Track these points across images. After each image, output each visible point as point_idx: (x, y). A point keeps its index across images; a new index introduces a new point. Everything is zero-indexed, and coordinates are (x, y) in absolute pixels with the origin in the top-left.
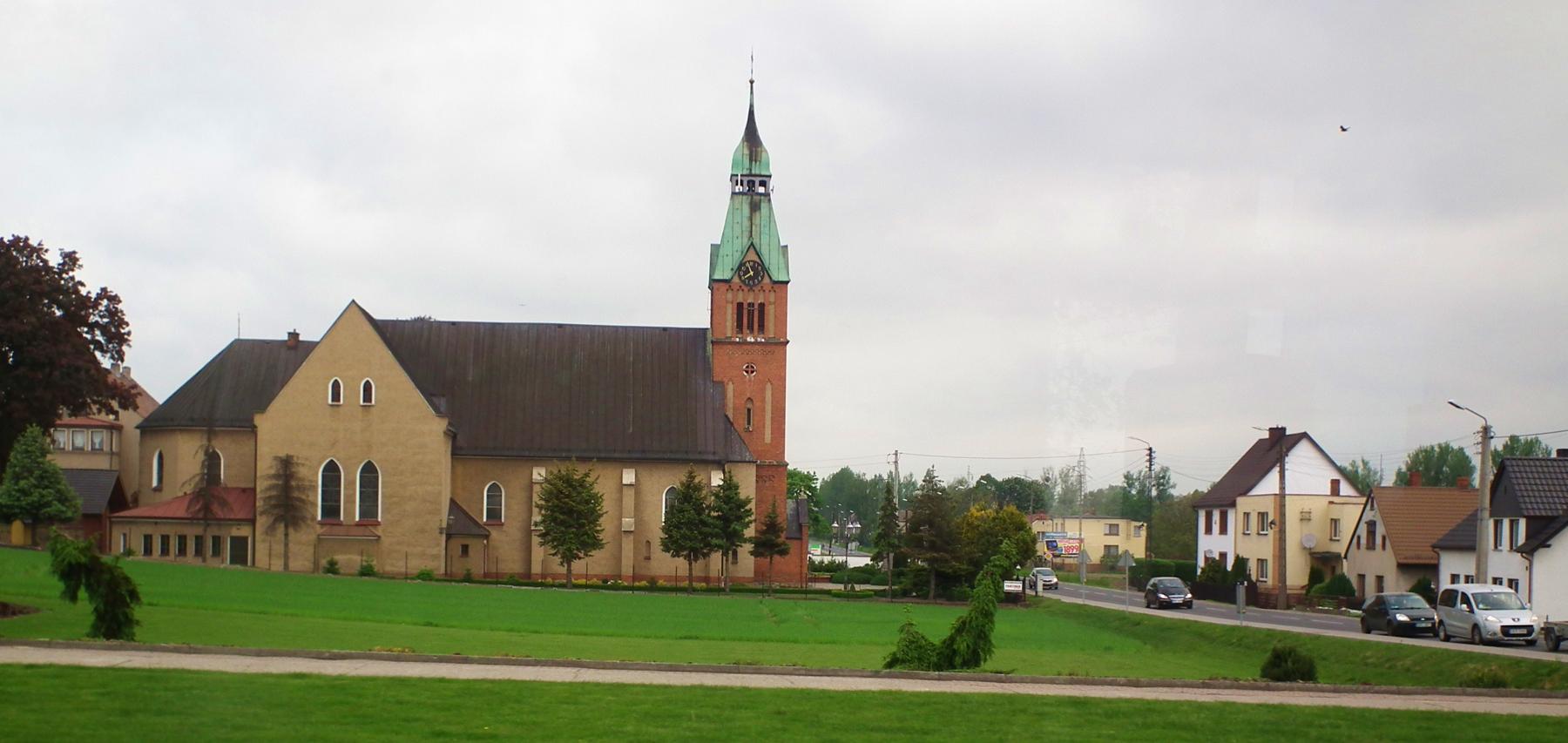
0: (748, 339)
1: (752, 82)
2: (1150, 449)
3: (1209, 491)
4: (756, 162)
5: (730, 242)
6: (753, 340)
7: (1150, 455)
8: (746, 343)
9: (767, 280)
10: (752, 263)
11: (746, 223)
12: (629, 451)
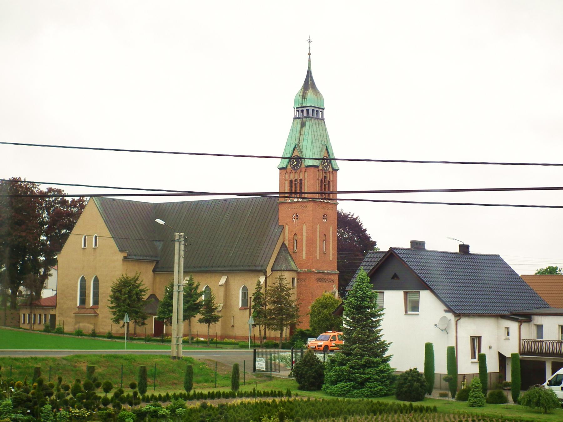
1: (309, 54)
3: (41, 291)
4: (305, 99)
5: (289, 146)
11: (298, 135)
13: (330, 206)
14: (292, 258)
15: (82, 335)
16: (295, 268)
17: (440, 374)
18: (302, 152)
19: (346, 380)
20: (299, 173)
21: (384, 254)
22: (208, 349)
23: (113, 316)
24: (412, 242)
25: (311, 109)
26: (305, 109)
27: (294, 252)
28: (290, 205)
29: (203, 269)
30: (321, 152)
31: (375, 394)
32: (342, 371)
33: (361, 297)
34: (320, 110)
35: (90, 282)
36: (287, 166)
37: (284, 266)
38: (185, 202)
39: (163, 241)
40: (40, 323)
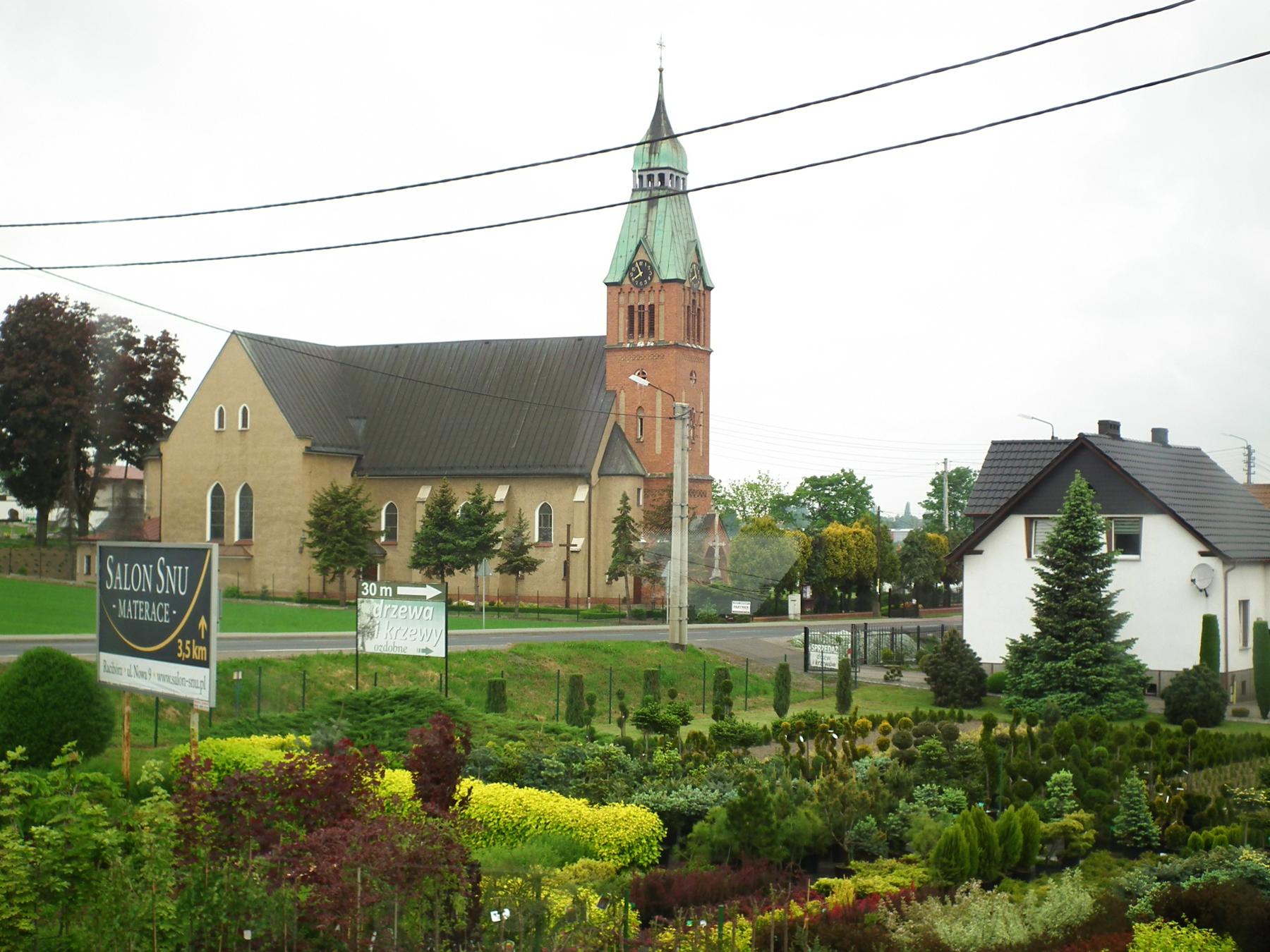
0: (639, 345)
1: (661, 70)
2: (1248, 448)
6: (642, 345)
7: (1249, 455)
8: (635, 348)
9: (656, 280)
10: (641, 263)
11: (642, 221)
12: (452, 468)
13: (700, 355)
14: (634, 453)
15: (268, 599)
16: (641, 471)
17: (1160, 671)
18: (652, 253)
19: (1065, 687)
20: (647, 292)
21: (1066, 446)
22: (530, 627)
23: (315, 562)
24: (1101, 423)
25: (667, 173)
26: (656, 173)
27: (638, 441)
28: (628, 353)
29: (458, 471)
30: (687, 254)
31: (1123, 714)
32: (1058, 672)
33: (1083, 529)
34: (681, 176)
35: (235, 495)
36: (622, 280)
37: (623, 466)
38: (402, 345)
39: (365, 418)
40: (89, 572)
